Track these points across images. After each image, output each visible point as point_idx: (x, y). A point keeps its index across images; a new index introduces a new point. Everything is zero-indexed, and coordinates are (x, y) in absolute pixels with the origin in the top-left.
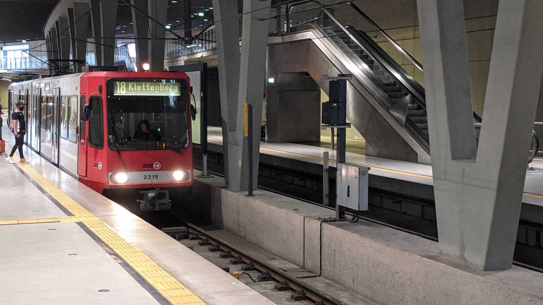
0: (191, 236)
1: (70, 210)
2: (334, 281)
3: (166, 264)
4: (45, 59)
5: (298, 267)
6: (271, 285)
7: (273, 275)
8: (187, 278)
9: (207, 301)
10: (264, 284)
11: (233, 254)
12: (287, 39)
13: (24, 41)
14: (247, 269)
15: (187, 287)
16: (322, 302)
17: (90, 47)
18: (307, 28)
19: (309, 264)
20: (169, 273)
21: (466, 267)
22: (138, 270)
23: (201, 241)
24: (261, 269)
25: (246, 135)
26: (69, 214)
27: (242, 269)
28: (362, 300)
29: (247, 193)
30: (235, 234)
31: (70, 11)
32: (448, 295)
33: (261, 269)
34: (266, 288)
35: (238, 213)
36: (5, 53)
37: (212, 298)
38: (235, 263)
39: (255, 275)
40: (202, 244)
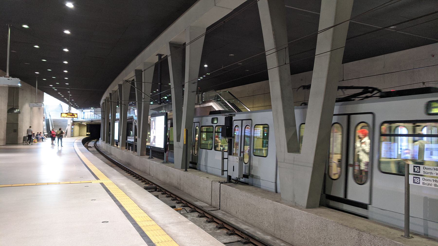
0: (158, 190)
1: (98, 177)
2: (227, 212)
3: (143, 206)
4: (100, 115)
5: (208, 205)
6: (196, 214)
7: (197, 210)
8: (153, 214)
9: (164, 228)
10: (193, 214)
11: (178, 199)
12: (202, 106)
13: (92, 108)
14: (184, 206)
15: (153, 220)
16: (233, 230)
17: (118, 110)
18: (210, 101)
19: (214, 204)
20: (144, 211)
21: (296, 206)
22: (127, 209)
23: (162, 192)
24: (191, 206)
25: (185, 143)
26: (97, 178)
27: (182, 206)
28: (241, 222)
29: (184, 170)
30: (178, 189)
31: (110, 94)
32: (287, 221)
33: (191, 206)
34: (193, 216)
35: (180, 179)
36: (84, 113)
37: (167, 227)
38: (178, 203)
39: (188, 209)
40: (163, 194)
